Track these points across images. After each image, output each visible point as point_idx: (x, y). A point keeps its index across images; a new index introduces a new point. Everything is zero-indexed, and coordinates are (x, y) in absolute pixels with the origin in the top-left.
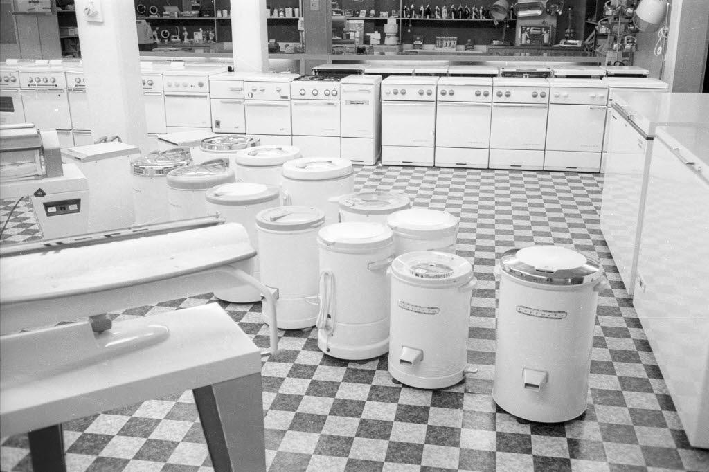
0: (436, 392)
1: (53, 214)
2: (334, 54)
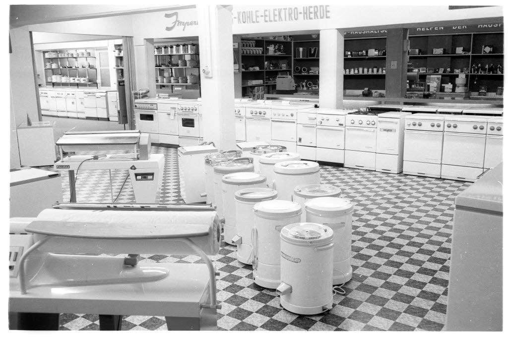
0: (301, 317)
1: (139, 180)
2: (406, 98)
